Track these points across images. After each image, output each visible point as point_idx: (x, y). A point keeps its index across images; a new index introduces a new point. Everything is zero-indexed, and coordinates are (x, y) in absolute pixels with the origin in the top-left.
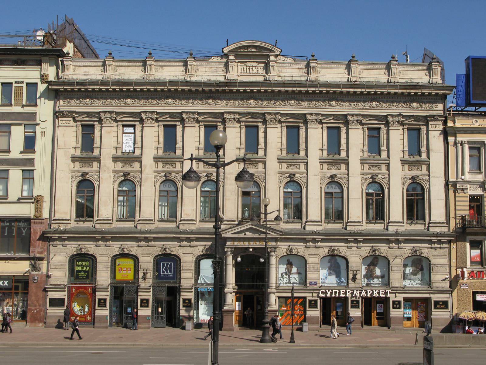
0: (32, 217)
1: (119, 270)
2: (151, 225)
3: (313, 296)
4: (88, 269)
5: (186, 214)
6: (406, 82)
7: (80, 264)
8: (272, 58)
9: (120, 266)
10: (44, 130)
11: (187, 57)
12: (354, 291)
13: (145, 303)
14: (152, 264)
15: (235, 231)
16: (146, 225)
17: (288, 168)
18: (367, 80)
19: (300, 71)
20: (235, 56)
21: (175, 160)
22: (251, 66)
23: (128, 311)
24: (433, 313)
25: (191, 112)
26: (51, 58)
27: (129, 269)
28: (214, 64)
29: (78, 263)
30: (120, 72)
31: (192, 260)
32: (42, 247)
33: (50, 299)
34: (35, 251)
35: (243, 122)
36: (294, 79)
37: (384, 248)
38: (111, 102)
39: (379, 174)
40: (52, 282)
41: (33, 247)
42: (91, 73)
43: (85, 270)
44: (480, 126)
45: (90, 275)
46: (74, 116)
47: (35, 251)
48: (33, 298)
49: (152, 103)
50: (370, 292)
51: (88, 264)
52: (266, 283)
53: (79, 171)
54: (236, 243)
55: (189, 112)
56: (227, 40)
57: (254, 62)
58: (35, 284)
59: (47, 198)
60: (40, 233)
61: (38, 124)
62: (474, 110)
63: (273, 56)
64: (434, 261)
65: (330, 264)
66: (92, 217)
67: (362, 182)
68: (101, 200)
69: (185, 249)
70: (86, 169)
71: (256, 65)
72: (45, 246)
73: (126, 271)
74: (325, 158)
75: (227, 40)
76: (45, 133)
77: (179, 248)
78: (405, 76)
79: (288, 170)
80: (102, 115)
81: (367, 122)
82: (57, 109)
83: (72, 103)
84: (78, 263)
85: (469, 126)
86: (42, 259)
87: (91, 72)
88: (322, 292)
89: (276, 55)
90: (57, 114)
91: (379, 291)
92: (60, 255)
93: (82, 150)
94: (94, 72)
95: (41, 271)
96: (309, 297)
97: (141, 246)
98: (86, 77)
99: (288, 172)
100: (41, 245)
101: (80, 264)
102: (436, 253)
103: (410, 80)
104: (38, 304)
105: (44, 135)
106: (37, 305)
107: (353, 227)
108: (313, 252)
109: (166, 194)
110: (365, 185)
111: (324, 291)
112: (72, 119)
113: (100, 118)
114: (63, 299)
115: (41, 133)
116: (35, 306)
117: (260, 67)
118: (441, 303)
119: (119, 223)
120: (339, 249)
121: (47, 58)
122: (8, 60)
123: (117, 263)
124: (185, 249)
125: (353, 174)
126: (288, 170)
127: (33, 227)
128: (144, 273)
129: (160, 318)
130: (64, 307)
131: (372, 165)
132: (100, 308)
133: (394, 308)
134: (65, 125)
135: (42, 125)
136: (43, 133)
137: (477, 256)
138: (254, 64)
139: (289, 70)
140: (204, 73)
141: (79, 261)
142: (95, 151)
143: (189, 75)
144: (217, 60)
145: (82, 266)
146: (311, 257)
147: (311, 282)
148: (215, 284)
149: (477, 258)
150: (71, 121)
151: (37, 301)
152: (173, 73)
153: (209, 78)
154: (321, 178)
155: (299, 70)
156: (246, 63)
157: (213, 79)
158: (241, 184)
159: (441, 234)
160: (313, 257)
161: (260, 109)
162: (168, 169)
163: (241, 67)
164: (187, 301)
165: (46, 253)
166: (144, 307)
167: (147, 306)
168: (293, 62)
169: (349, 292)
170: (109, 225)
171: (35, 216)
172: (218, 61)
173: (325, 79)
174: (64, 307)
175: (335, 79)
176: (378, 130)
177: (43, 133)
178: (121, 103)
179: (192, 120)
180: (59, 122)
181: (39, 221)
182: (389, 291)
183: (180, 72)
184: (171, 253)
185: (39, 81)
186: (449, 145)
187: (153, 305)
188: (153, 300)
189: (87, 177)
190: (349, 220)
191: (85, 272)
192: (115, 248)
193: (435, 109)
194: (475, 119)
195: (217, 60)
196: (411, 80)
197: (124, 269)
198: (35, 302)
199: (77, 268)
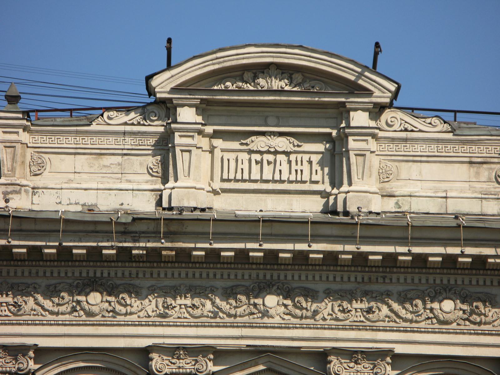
22: (268, 152)
28: (110, 142)
36: (453, 206)
56: (169, 41)
57: (281, 134)
75: (169, 41)
89: (376, 104)
138: (282, 143)
144: (125, 124)
153: (89, 198)
156: (248, 141)
168: (450, 136)
172: (128, 128)
195: (125, 124)
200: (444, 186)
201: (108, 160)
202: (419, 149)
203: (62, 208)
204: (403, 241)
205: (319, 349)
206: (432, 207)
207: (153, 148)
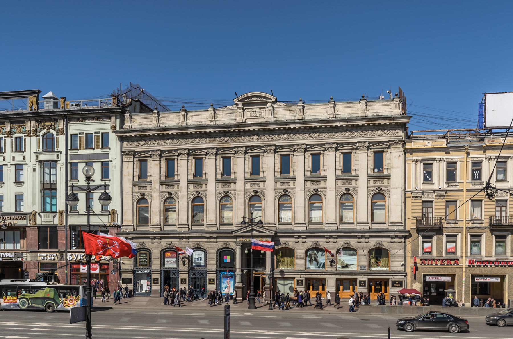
5: (210, 220)
6: (373, 115)
8: (270, 104)
10: (114, 165)
11: (360, 99)
13: (183, 281)
15: (242, 232)
16: (155, 229)
18: (341, 116)
19: (291, 112)
20: (243, 105)
21: (147, 184)
24: (208, 287)
25: (212, 148)
26: (117, 115)
28: (228, 112)
30: (163, 121)
35: (340, 150)
36: (286, 119)
37: (148, 243)
39: (173, 191)
44: (433, 147)
46: (134, 154)
48: (112, 278)
52: (251, 268)
53: (138, 193)
54: (243, 239)
55: (211, 148)
56: (271, 91)
57: (257, 108)
59: (119, 212)
61: (111, 161)
62: (505, 131)
64: (392, 251)
66: (148, 223)
68: (153, 212)
70: (143, 191)
71: (259, 110)
74: (309, 177)
75: (271, 91)
78: (373, 111)
85: (423, 147)
89: (272, 101)
90: (123, 153)
93: (311, 172)
94: (145, 122)
98: (140, 127)
99: (282, 188)
102: (394, 245)
103: (376, 113)
107: (330, 227)
114: (131, 278)
116: (114, 283)
118: (397, 283)
121: (114, 114)
122: (89, 117)
125: (330, 188)
131: (344, 181)
134: (128, 161)
135: (114, 162)
137: (428, 248)
138: (258, 110)
139: (283, 112)
142: (290, 173)
149: (429, 249)
151: (115, 280)
152: (199, 120)
153: (224, 122)
157: (227, 123)
158: (101, 201)
159: (399, 231)
161: (261, 143)
162: (197, 189)
164: (212, 280)
166: (362, 286)
168: (286, 106)
172: (231, 109)
173: (310, 118)
175: (317, 117)
185: (110, 131)
186: (407, 163)
189: (145, 196)
190: (123, 225)
192: (164, 243)
193: (397, 135)
194: (428, 141)
196: (378, 113)
200: (285, 115)
201: (228, 115)
202: (281, 109)
203: (220, 124)
204: (226, 128)
205: (25, 141)
206: (283, 119)
207: (65, 120)
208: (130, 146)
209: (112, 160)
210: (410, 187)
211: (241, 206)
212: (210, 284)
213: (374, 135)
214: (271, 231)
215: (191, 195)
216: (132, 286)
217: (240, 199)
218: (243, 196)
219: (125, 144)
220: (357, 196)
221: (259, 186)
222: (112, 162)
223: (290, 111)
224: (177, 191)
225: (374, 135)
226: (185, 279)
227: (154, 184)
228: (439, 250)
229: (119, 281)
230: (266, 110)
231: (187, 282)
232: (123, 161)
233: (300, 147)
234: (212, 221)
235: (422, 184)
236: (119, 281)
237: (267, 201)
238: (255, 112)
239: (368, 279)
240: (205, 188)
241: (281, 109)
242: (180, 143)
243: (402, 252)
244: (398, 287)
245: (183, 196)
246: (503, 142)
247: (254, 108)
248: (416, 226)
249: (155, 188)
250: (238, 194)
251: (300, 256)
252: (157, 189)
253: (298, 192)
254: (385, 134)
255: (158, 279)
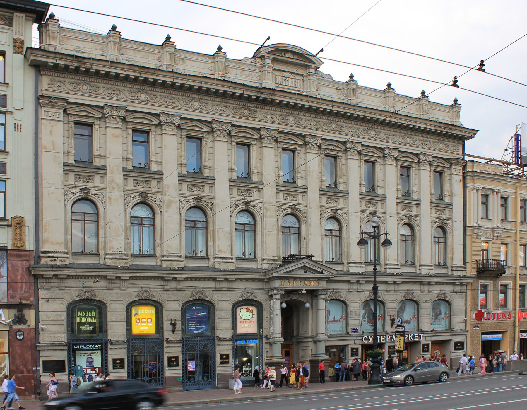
0: (9, 247)
1: (136, 322)
2: (181, 263)
3: (355, 344)
4: (94, 320)
7: (83, 314)
9: (137, 317)
10: (19, 123)
12: (392, 336)
14: (65, 313)
17: (285, 198)
19: (338, 92)
20: (274, 60)
23: (190, 369)
27: (149, 320)
29: (79, 312)
30: (129, 57)
31: (229, 306)
32: (26, 290)
33: (44, 361)
34: (15, 297)
38: (224, 111)
40: (44, 338)
41: (12, 291)
42: (85, 50)
43: (91, 323)
45: (97, 329)
47: (15, 297)
49: (174, 105)
50: (388, 337)
51: (93, 314)
58: (20, 342)
60: (23, 270)
63: (314, 69)
65: (364, 310)
67: (181, 206)
69: (221, 293)
72: (30, 289)
73: (145, 322)
76: (21, 126)
77: (348, 293)
79: (329, 205)
80: (386, 152)
81: (401, 159)
82: (40, 93)
83: (396, 139)
84: (79, 312)
86: (28, 306)
87: (87, 49)
88: (365, 339)
91: (414, 335)
92: (55, 302)
94: (90, 50)
95: (28, 323)
96: (351, 344)
97: (63, 288)
99: (329, 207)
100: (24, 287)
101: (83, 314)
104: (26, 369)
105: (19, 129)
106: (25, 370)
108: (355, 297)
109: (242, 227)
110: (185, 209)
111: (367, 337)
112: (62, 111)
113: (384, 154)
114: (64, 361)
115: (15, 125)
116: (22, 372)
117: (296, 80)
119: (239, 262)
120: (204, 291)
121: (24, 15)
123: (133, 312)
124: (221, 293)
125: (390, 214)
126: (329, 205)
127: (11, 261)
128: (391, 320)
129: (153, 381)
130: (65, 372)
132: (115, 371)
133: (170, 365)
134: (52, 118)
135: (17, 115)
136: (18, 126)
140: (236, 77)
141: (81, 310)
143: (221, 75)
145: (85, 316)
146: (353, 302)
147: (354, 329)
148: (374, 333)
150: (60, 113)
151: (25, 366)
154: (361, 216)
155: (337, 91)
160: (354, 302)
161: (301, 129)
163: (276, 77)
164: (224, 357)
165: (32, 299)
167: (177, 365)
169: (388, 337)
170: (124, 261)
171: (14, 245)
174: (65, 372)
176: (146, 135)
177: (18, 126)
178: (326, 128)
179: (271, 140)
180: (43, 113)
181: (20, 253)
182: (421, 335)
183: (207, 70)
184: (204, 298)
187: (128, 366)
188: (128, 360)
191: (90, 324)
193: (457, 153)
194: (489, 167)
197: (143, 320)
198: (21, 367)
199: (79, 320)
201: (246, 72)
202: (324, 83)
208: (56, 90)
209: (12, 110)
210: (470, 224)
211: (272, 229)
212: (221, 363)
213: (133, 98)
214: (332, 271)
215: (185, 203)
216: (181, 372)
217: (270, 217)
218: (274, 214)
219: (45, 81)
220: (419, 228)
221: (295, 199)
222: (13, 116)
223: (337, 89)
224: (157, 192)
225: (133, 98)
226: (177, 358)
227: (112, 173)
228: (496, 302)
229: (34, 368)
230: (303, 80)
231: (180, 363)
232: (40, 117)
233: (354, 146)
234: (225, 252)
235: (482, 218)
236: (34, 368)
237: (310, 225)
238: (288, 79)
239: (432, 341)
240: (208, 192)
241: (324, 83)
242: (163, 103)
243: (462, 305)
244: (460, 349)
245: (169, 205)
246: (181, 153)
247: (285, 71)
248: (477, 272)
249: (113, 181)
250: (266, 209)
251: (356, 311)
252: (118, 185)
253: (351, 215)
254: (152, 101)
255: (122, 360)
